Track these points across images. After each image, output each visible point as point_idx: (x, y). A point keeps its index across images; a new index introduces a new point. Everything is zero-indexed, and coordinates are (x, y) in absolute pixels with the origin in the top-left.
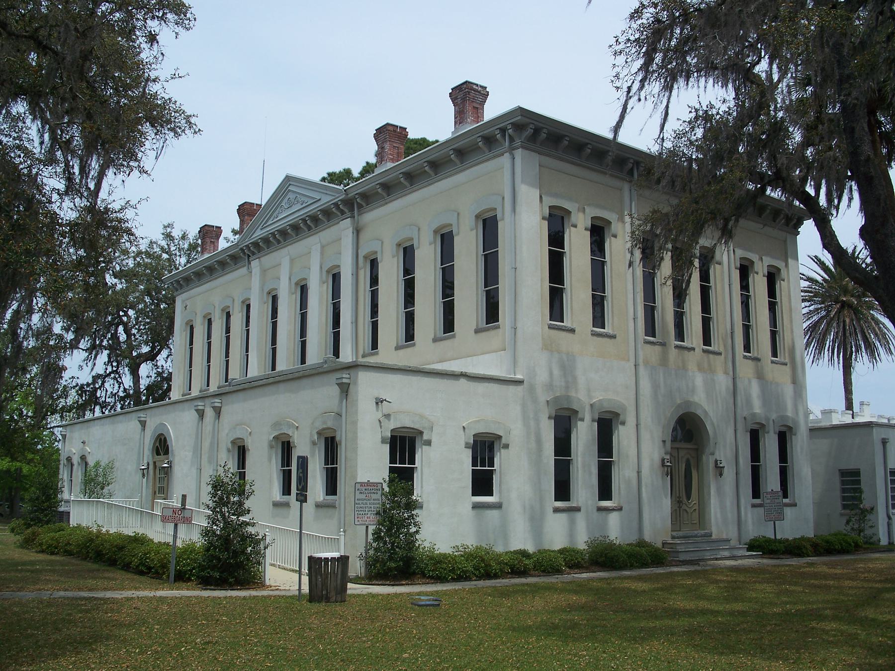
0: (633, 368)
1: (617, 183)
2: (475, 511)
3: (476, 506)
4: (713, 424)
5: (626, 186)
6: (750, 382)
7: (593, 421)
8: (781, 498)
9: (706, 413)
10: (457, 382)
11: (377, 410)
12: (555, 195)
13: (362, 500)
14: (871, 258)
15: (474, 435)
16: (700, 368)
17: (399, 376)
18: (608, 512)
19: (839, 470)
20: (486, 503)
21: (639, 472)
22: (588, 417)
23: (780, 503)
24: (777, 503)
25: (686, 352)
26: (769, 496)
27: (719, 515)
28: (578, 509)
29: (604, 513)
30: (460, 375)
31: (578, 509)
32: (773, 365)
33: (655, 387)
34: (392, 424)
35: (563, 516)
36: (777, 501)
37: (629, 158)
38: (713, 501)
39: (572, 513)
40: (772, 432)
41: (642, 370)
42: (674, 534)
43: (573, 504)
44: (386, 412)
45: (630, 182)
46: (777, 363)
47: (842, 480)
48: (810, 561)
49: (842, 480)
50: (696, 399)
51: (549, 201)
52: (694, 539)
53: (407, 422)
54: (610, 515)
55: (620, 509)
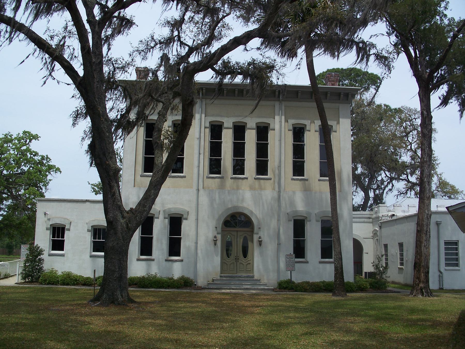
0: (195, 192)
1: (272, 103)
2: (91, 259)
3: (92, 256)
4: (257, 217)
5: (277, 104)
6: (294, 193)
7: (165, 218)
8: (294, 258)
9: (252, 212)
10: (84, 204)
11: (45, 217)
12: (293, 118)
13: (23, 252)
14: (106, 97)
15: (92, 226)
16: (252, 188)
17: (56, 203)
18: (173, 262)
19: (399, 243)
20: (97, 255)
21: (197, 243)
22: (161, 216)
23: (293, 261)
24: (292, 261)
25: (240, 180)
26: (288, 257)
27: (261, 267)
28: (153, 260)
29: (170, 263)
30: (86, 201)
31: (153, 260)
32: (321, 182)
33: (212, 201)
34: (51, 223)
35: (143, 263)
36: (292, 260)
37: (235, 89)
38: (256, 259)
39: (149, 262)
40: (314, 221)
41: (202, 192)
42: (222, 275)
43: (153, 257)
44: (49, 218)
45: (279, 100)
46: (324, 181)
47: (457, 251)
48: (368, 296)
49: (457, 251)
50: (245, 205)
51: (292, 122)
52: (239, 278)
53: (58, 221)
54: (175, 263)
55: (182, 261)
